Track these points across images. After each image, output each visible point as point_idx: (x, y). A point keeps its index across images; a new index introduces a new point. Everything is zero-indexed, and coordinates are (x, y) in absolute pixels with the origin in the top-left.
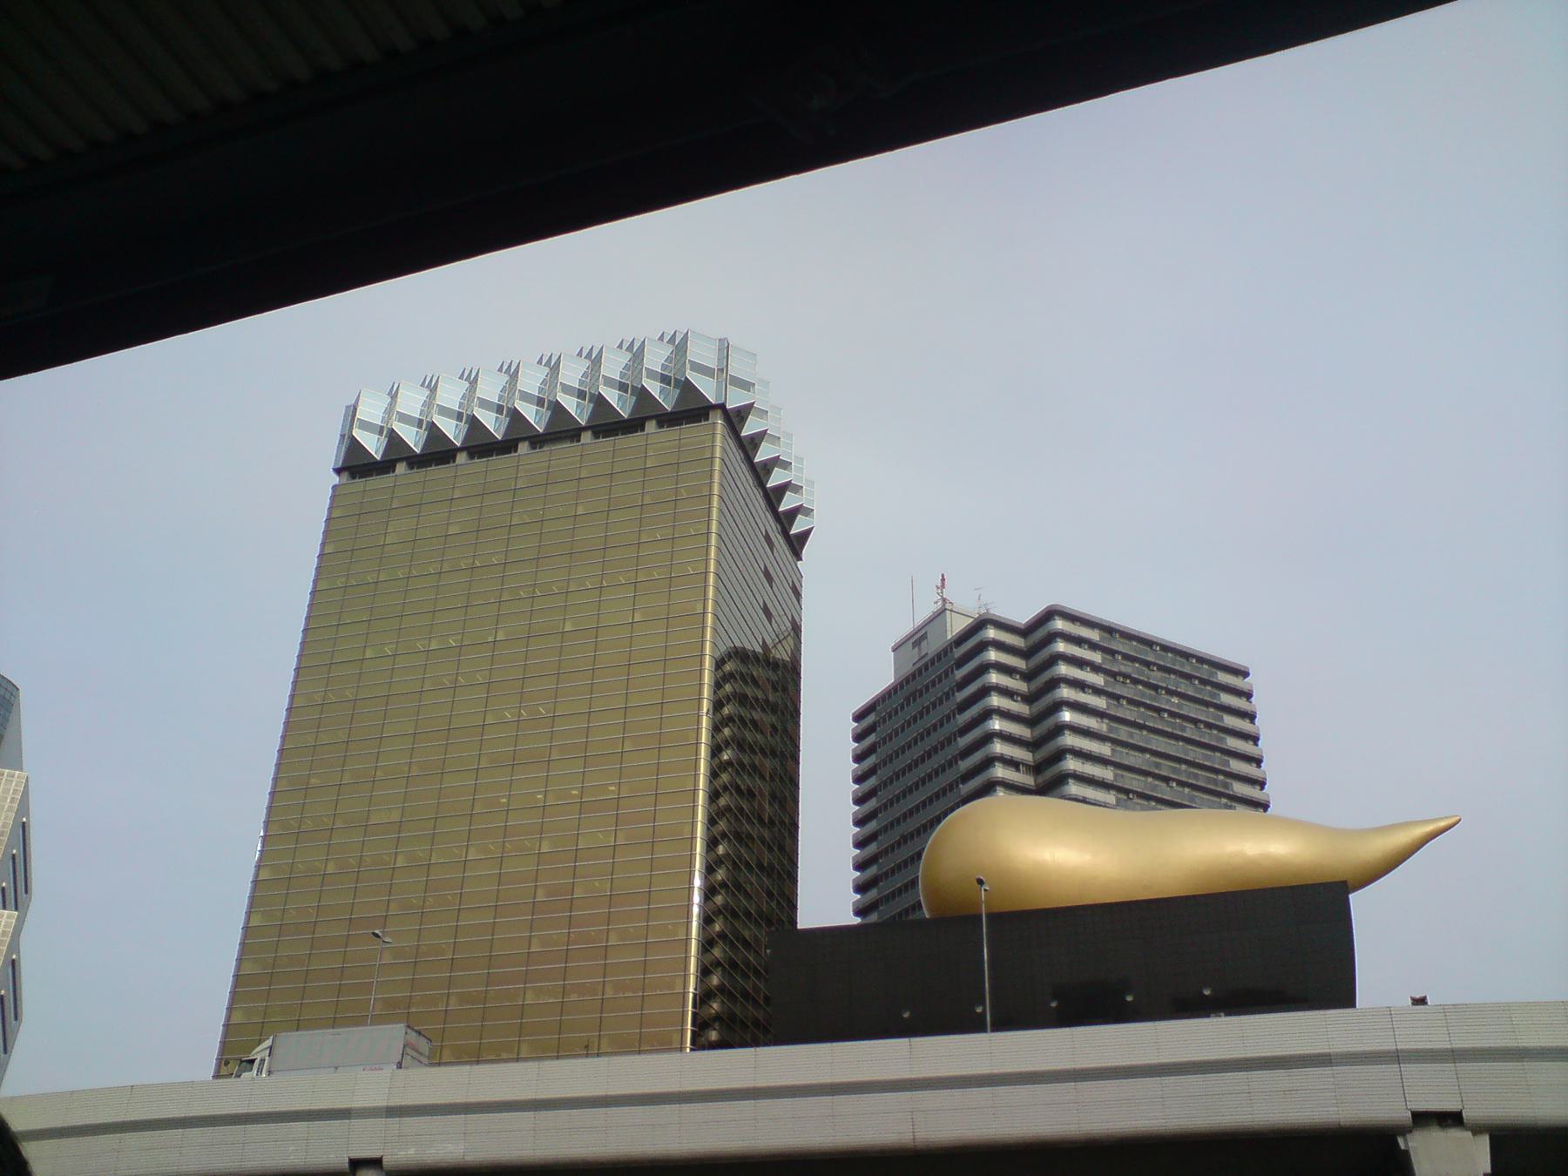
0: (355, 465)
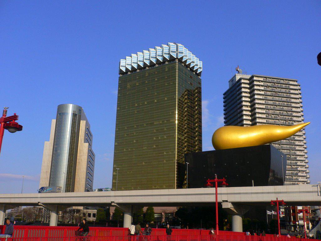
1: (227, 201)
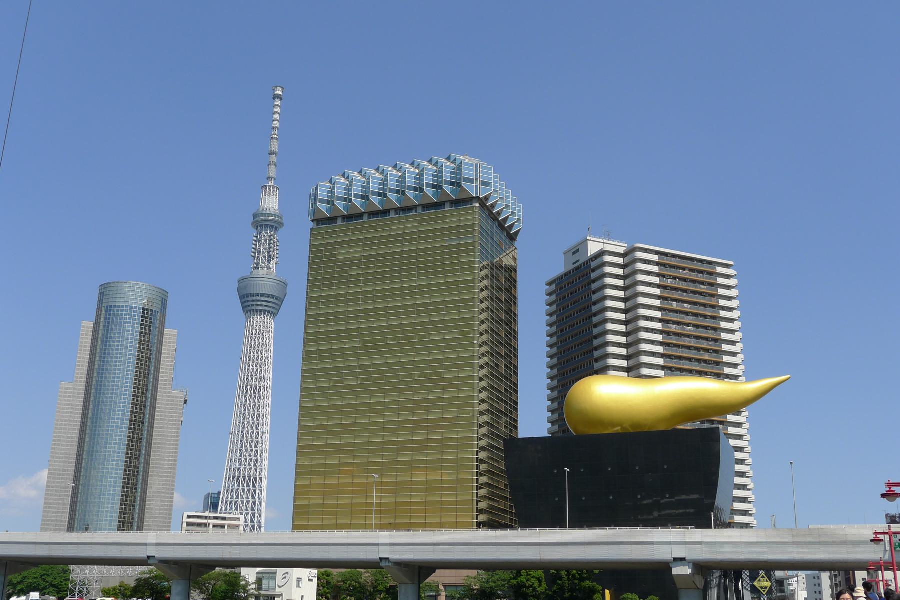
0: (320, 221)
1: (683, 559)
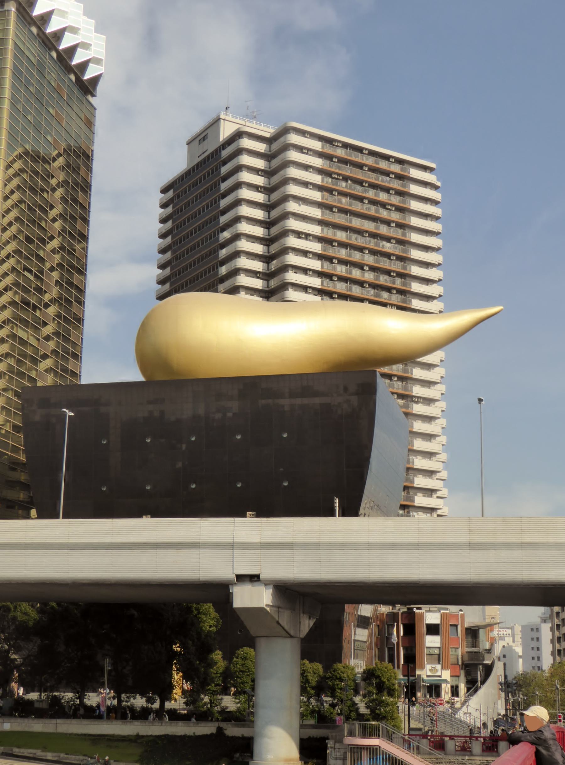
1: (254, 578)
